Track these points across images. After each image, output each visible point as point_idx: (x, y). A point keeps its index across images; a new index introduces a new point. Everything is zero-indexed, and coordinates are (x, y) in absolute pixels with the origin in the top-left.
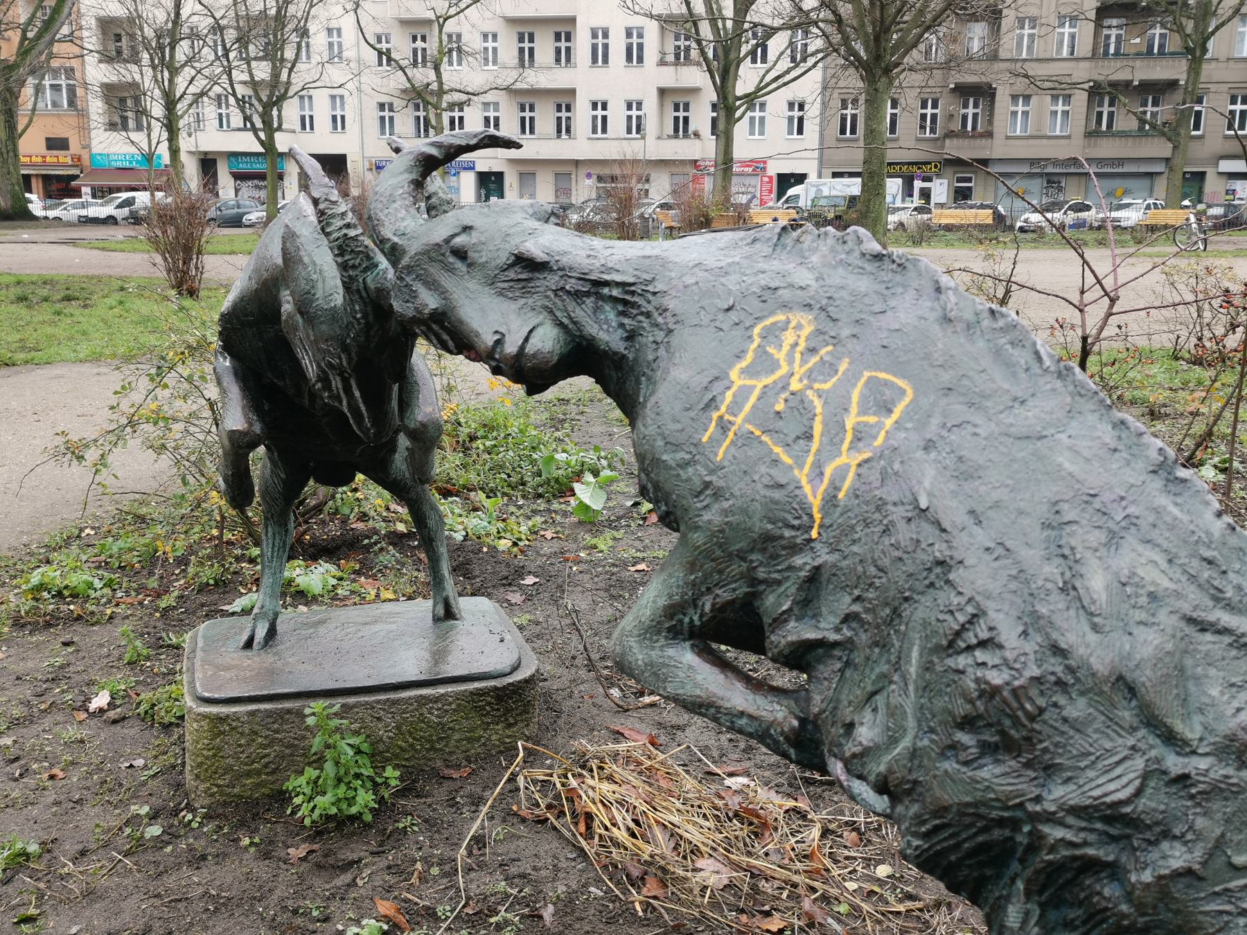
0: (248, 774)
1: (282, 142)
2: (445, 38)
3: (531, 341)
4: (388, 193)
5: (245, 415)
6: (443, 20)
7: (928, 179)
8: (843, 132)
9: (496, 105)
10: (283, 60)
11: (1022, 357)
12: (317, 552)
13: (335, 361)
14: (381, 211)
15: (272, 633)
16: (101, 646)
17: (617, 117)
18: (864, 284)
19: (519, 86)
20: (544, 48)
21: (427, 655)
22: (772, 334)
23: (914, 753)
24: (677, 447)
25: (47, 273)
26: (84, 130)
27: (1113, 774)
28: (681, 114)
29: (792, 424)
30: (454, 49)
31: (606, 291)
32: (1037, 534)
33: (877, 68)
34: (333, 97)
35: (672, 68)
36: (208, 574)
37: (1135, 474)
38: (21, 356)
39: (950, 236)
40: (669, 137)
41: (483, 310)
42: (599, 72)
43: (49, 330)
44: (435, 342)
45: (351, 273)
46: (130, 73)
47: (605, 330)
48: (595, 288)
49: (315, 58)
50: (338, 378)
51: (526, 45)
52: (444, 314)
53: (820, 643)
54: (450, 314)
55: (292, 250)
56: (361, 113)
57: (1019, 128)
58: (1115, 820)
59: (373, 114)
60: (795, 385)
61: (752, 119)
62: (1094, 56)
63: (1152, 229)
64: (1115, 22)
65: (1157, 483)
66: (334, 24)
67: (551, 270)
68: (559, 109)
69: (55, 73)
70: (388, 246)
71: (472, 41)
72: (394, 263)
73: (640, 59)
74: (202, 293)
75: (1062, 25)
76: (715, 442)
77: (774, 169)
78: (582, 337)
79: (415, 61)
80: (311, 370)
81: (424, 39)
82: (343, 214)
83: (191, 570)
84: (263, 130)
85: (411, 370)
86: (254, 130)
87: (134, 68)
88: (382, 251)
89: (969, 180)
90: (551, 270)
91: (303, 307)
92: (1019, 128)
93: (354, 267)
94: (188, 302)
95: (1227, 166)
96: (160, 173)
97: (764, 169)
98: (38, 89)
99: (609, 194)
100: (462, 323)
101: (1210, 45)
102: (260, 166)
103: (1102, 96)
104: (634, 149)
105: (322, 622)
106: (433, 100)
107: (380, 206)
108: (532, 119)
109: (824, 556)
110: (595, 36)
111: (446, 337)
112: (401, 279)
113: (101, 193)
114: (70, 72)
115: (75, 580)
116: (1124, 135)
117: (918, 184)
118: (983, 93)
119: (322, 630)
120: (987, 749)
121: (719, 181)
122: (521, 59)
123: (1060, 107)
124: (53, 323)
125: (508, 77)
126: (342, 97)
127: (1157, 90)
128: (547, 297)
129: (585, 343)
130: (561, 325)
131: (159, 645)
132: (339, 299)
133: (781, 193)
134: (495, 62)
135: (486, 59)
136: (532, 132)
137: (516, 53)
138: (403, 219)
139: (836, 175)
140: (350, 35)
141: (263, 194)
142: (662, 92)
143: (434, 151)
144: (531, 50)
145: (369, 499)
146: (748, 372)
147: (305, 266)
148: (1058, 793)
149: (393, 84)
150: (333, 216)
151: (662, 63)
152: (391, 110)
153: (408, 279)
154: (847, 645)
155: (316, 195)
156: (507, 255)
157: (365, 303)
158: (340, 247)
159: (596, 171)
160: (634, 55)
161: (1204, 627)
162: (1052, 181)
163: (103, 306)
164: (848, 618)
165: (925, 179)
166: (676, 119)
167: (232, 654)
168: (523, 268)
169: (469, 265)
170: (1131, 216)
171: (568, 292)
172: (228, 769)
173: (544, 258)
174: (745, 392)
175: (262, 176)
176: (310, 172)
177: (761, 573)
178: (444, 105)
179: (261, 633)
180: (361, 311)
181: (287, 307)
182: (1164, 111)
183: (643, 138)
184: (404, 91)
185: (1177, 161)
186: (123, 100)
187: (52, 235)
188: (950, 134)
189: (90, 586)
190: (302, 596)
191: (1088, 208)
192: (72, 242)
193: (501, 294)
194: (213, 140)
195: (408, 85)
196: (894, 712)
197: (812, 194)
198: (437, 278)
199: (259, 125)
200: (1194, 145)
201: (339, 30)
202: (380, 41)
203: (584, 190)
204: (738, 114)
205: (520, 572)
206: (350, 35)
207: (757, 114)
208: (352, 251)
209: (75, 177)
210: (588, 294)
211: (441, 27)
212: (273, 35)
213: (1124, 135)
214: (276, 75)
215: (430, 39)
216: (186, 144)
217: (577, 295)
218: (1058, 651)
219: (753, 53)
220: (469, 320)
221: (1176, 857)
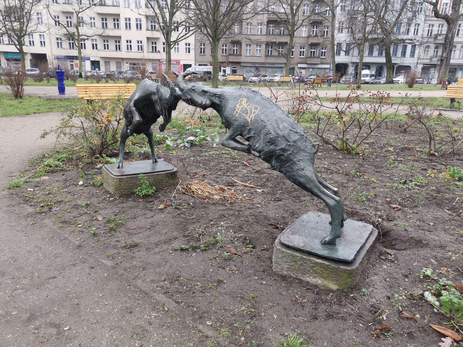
0: (126, 189)
8: (201, 53)
9: (96, 40)
11: (272, 103)
17: (135, 45)
18: (252, 95)
19: (103, 34)
20: (110, 23)
22: (241, 101)
23: (263, 147)
24: (231, 115)
27: (283, 145)
29: (246, 111)
30: (80, 22)
32: (275, 122)
33: (215, 39)
34: (40, 35)
35: (151, 31)
37: (284, 116)
39: (232, 83)
40: (151, 52)
42: (128, 31)
47: (217, 101)
48: (215, 95)
51: (104, 22)
53: (251, 137)
58: (283, 150)
59: (55, 42)
62: (267, 35)
63: (282, 82)
64: (272, 26)
68: (116, 42)
71: (87, 19)
73: (141, 28)
77: (182, 63)
81: (70, 18)
84: (18, 45)
89: (236, 68)
95: (300, 66)
97: (179, 63)
101: (295, 33)
102: (19, 57)
103: (269, 46)
104: (139, 55)
109: (251, 127)
110: (126, 20)
116: (275, 56)
117: (222, 68)
118: (238, 43)
120: (271, 145)
121: (167, 66)
122: (103, 26)
123: (258, 48)
125: (100, 32)
126: (43, 35)
127: (282, 45)
134: (95, 27)
135: (92, 26)
137: (101, 24)
139: (200, 65)
142: (148, 38)
144: (106, 23)
148: (278, 148)
149: (62, 32)
151: (147, 30)
154: (254, 137)
160: (139, 27)
161: (291, 130)
162: (257, 68)
165: (224, 67)
166: (153, 47)
170: (277, 79)
172: (123, 188)
182: (283, 51)
183: (143, 52)
184: (65, 35)
185: (287, 64)
188: (230, 55)
191: (266, 76)
195: (67, 33)
199: (17, 43)
200: (292, 60)
201: (41, 13)
202: (55, 18)
203: (126, 67)
204: (172, 47)
213: (275, 56)
217: (212, 96)
218: (277, 134)
221: (289, 152)
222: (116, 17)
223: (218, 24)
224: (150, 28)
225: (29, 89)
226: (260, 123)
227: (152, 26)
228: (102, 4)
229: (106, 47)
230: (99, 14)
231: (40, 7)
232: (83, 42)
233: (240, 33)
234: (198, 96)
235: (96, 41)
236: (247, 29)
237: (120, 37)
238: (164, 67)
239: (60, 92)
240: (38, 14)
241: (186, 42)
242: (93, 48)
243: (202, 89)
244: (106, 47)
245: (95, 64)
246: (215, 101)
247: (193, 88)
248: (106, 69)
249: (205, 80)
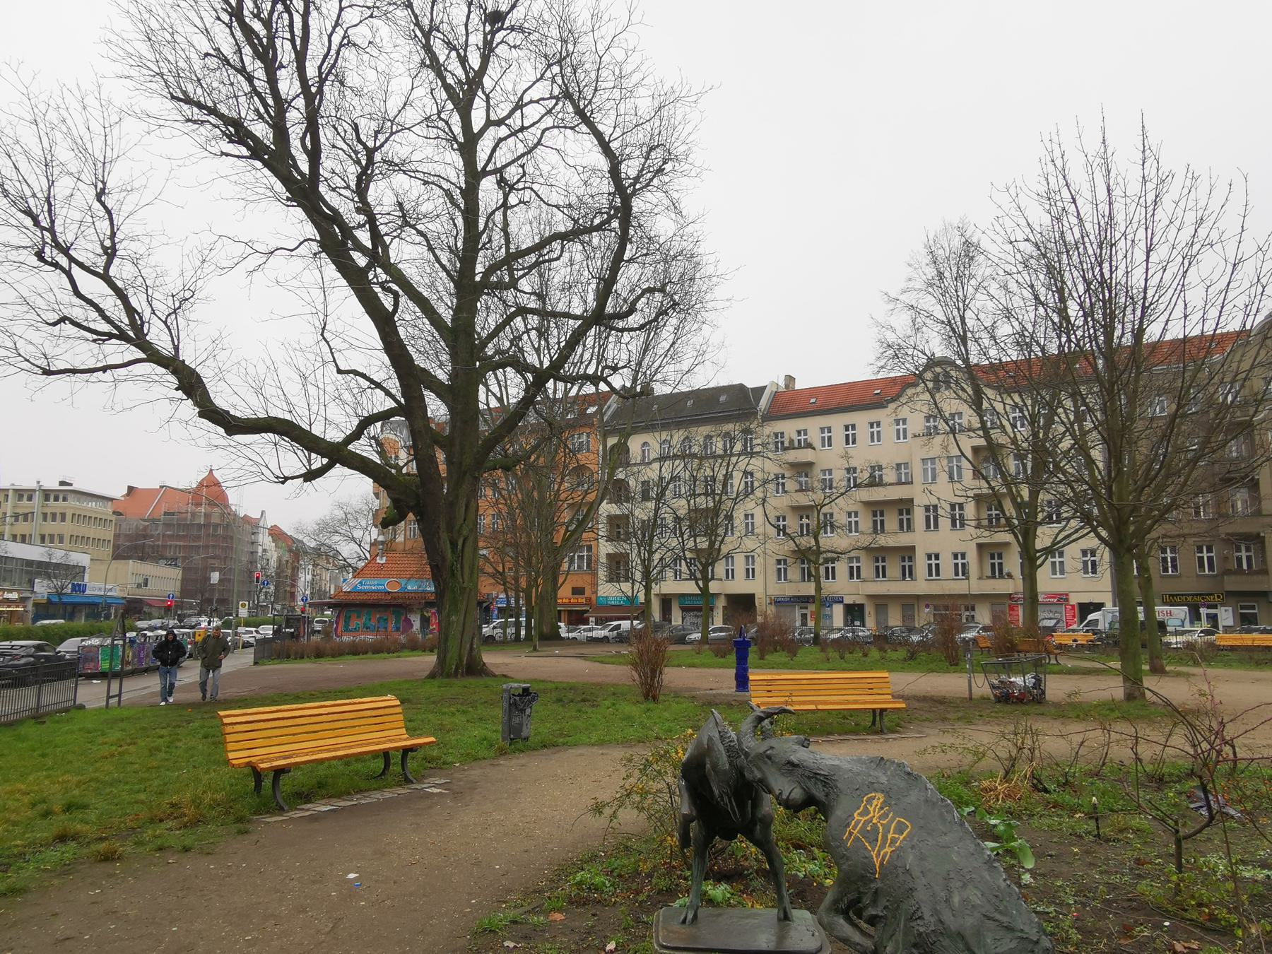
1: (714, 587)
2: (822, 517)
10: (717, 535)
12: (721, 877)
15: (695, 917)
20: (891, 522)
21: (774, 938)
22: (870, 801)
26: (595, 585)
28: (996, 561)
29: (871, 834)
30: (828, 524)
34: (747, 557)
36: (663, 884)
39: (1232, 656)
40: (988, 578)
46: (624, 547)
47: (819, 793)
49: (737, 534)
59: (772, 567)
60: (875, 821)
61: (1054, 564)
65: (986, 867)
71: (840, 518)
74: (661, 698)
76: (848, 839)
77: (1075, 600)
79: (802, 531)
80: (716, 793)
83: (654, 881)
86: (696, 580)
87: (627, 547)
89: (1253, 608)
91: (715, 766)
94: (652, 705)
96: (637, 608)
97: (1067, 600)
98: (571, 561)
102: (699, 603)
104: (959, 587)
105: (720, 915)
106: (813, 558)
108: (884, 567)
109: (880, 885)
113: (602, 621)
114: (590, 548)
117: (1203, 611)
124: (577, 718)
125: (866, 540)
131: (638, 921)
133: (1083, 618)
136: (884, 576)
137: (871, 525)
140: (759, 518)
141: (700, 621)
145: (744, 847)
146: (861, 814)
152: (785, 563)
159: (936, 602)
161: (989, 918)
164: (885, 907)
165: (1208, 607)
166: (993, 565)
167: (676, 926)
174: (859, 821)
175: (699, 609)
177: (861, 889)
178: (821, 561)
179: (690, 916)
181: (708, 766)
183: (968, 579)
184: (794, 552)
186: (618, 563)
187: (571, 651)
188: (1228, 572)
189: (604, 884)
190: (711, 902)
194: (670, 585)
196: (897, 941)
199: (699, 575)
204: (1039, 562)
206: (759, 518)
207: (1057, 560)
209: (586, 611)
211: (819, 512)
214: (712, 544)
216: (656, 589)
217: (809, 778)
218: (941, 922)
222: (905, 507)
224: (985, 523)
225: (673, 676)
226: (902, 877)
229: (881, 572)
230: (867, 504)
232: (830, 565)
235: (858, 561)
237: (912, 549)
239: (738, 686)
240: (746, 516)
241: (1085, 547)
242: (852, 576)
244: (881, 572)
245: (854, 612)
246: (814, 791)
248: (878, 623)
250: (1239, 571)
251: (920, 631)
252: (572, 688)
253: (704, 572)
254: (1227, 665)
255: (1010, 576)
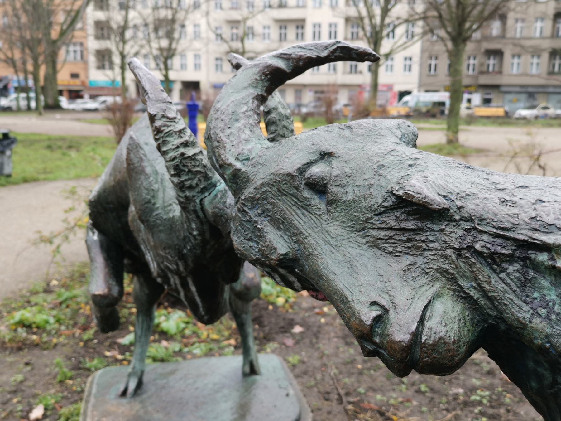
1: (172, 75)
3: (428, 324)
4: (230, 110)
5: (106, 282)
6: (245, 20)
7: (470, 93)
13: (173, 267)
14: (223, 130)
15: (140, 384)
16: (46, 366)
25: (63, 134)
26: (86, 69)
30: (250, 33)
31: (532, 254)
33: (459, 38)
38: (42, 176)
41: (350, 265)
43: (59, 163)
44: (278, 280)
45: (188, 193)
49: (188, 38)
50: (176, 277)
52: (295, 260)
54: (303, 261)
55: (135, 161)
56: (208, 62)
57: (515, 69)
59: (213, 63)
61: (387, 66)
66: (197, 22)
67: (451, 220)
69: (75, 44)
70: (229, 172)
71: (259, 29)
72: (236, 193)
75: (536, 21)
78: (501, 318)
82: (181, 132)
85: (243, 266)
86: (160, 70)
88: (222, 176)
90: (451, 220)
92: (515, 69)
93: (191, 188)
98: (68, 52)
99: (319, 99)
100: (320, 277)
105: (172, 372)
107: (221, 125)
111: (292, 278)
112: (244, 212)
113: (93, 97)
114: (81, 44)
115: (40, 318)
118: (498, 54)
119: (171, 379)
124: (60, 159)
128: (446, 257)
129: (503, 327)
130: (467, 299)
132: (176, 211)
138: (247, 141)
140: (204, 27)
143: (281, 64)
147: (147, 176)
150: (169, 134)
153: (251, 213)
155: (152, 111)
156: (383, 193)
157: (202, 223)
158: (176, 168)
162: (531, 95)
163: (86, 150)
168: (408, 214)
169: (330, 203)
171: (479, 254)
173: (444, 203)
176: (147, 87)
179: (132, 385)
180: (197, 229)
188: (482, 73)
189: (47, 322)
192: (78, 120)
193: (375, 244)
197: (415, 100)
198: (288, 215)
205: (291, 324)
206: (204, 27)
208: (190, 171)
210: (510, 259)
212: (167, 27)
215: (240, 30)
217: (494, 260)
219: (388, 35)
220: (331, 276)
223: (468, 10)
227: (353, 33)
228: (282, 6)
230: (277, 21)
231: (197, 17)
233: (503, 36)
234: (355, 250)
236: (516, 29)
238: (366, 95)
243: (392, 180)
246: (519, 310)
247: (316, 170)
249: (434, 116)
250: (487, 72)
251: (306, 106)
252: (63, 139)
253: (165, 64)
254: (484, 125)
255: (361, 72)
